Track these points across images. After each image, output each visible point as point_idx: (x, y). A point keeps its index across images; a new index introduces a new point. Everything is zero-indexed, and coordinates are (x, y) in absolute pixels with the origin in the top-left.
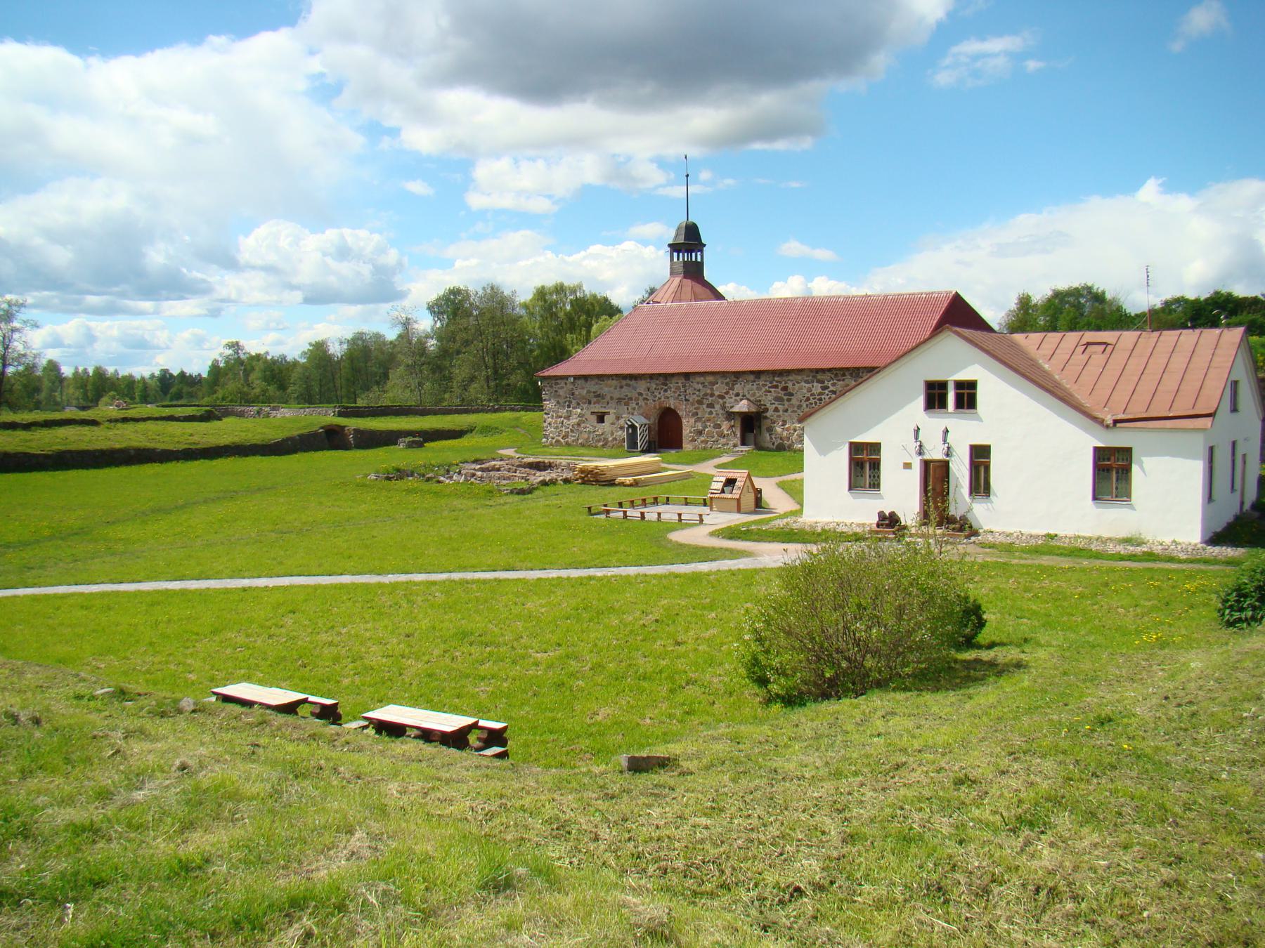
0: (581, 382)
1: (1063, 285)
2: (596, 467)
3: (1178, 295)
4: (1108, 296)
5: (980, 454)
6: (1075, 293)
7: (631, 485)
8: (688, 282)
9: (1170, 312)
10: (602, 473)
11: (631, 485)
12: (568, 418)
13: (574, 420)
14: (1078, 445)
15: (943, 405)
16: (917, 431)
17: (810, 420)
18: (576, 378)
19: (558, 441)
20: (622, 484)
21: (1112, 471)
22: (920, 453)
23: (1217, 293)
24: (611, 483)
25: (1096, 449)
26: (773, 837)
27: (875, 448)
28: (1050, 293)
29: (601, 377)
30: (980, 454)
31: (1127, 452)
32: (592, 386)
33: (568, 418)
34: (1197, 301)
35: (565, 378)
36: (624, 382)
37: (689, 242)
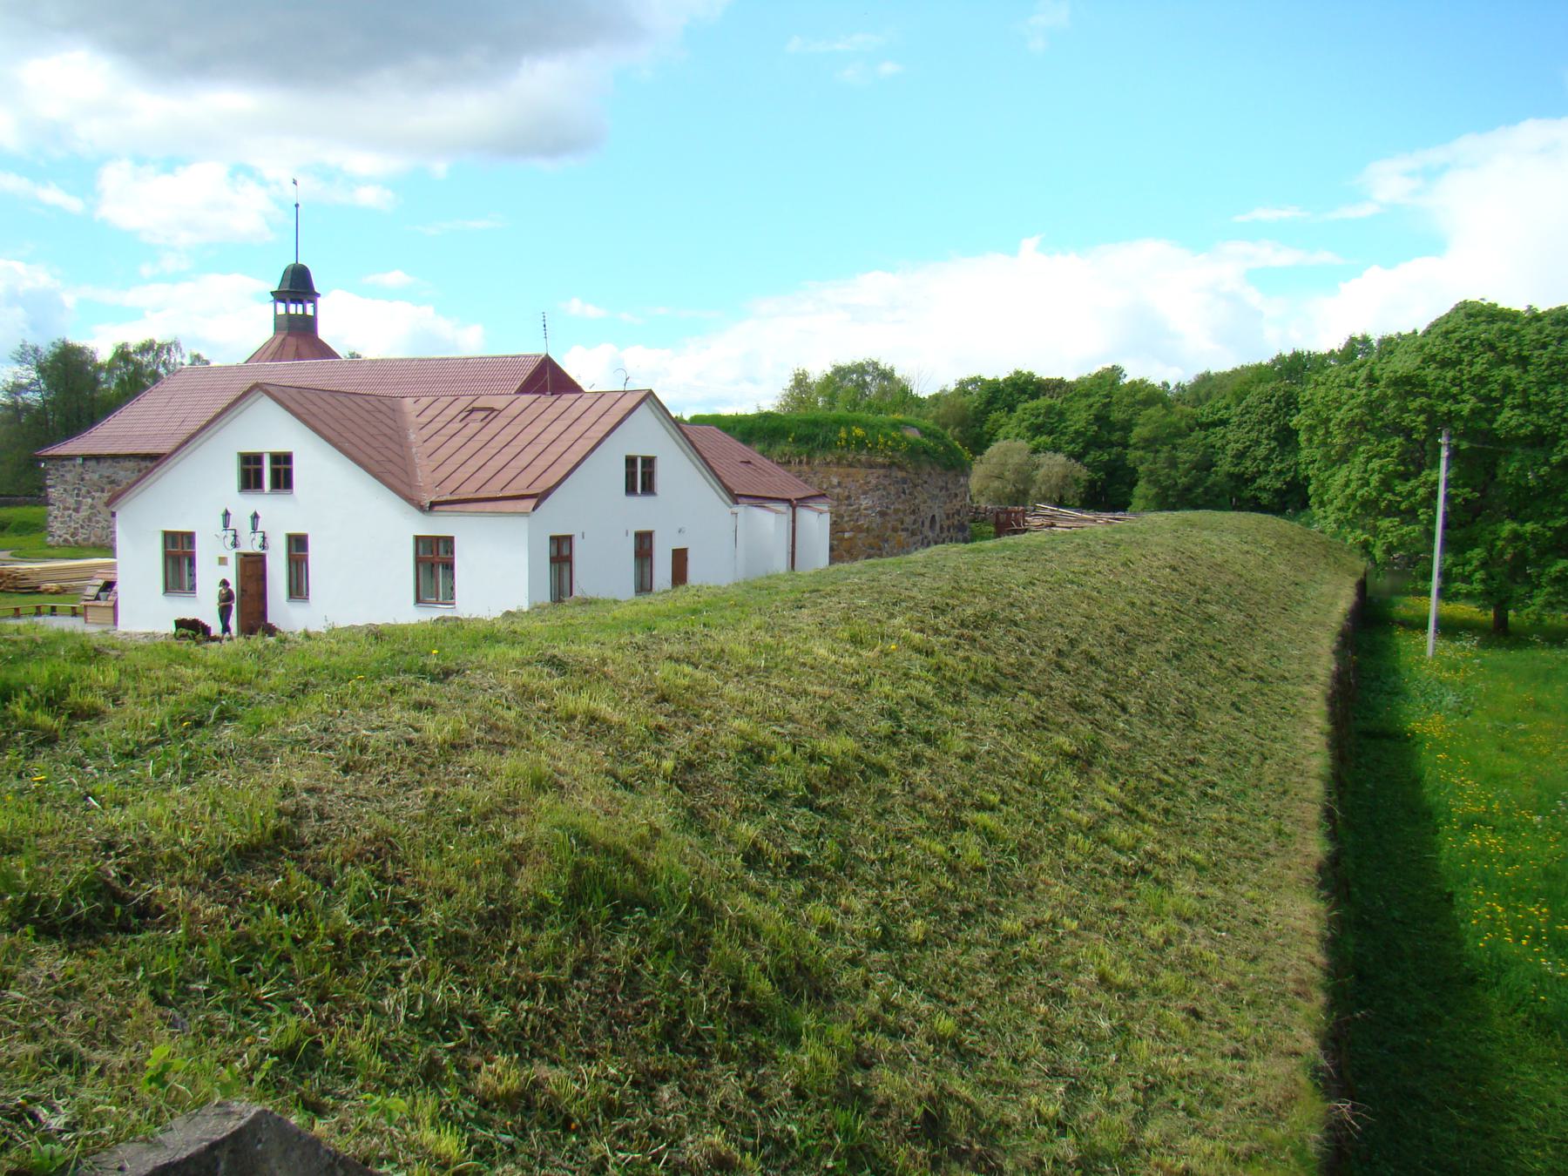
0: (92, 464)
1: (846, 361)
2: (33, 572)
3: (974, 374)
4: (897, 375)
5: (298, 544)
6: (861, 369)
7: (57, 593)
8: (292, 341)
9: (966, 393)
10: (24, 577)
11: (57, 593)
12: (77, 510)
13: (84, 513)
14: (396, 528)
15: (258, 485)
16: (227, 514)
17: (122, 501)
18: (86, 458)
19: (66, 540)
20: (47, 592)
21: (434, 560)
22: (235, 545)
23: (1017, 373)
24: (35, 590)
25: (418, 539)
26: (1300, 982)
27: (190, 537)
28: (829, 370)
29: (115, 457)
30: (298, 544)
31: (449, 541)
32: (106, 469)
33: (77, 510)
34: (995, 382)
35: (71, 458)
36: (143, 464)
37: (298, 285)
